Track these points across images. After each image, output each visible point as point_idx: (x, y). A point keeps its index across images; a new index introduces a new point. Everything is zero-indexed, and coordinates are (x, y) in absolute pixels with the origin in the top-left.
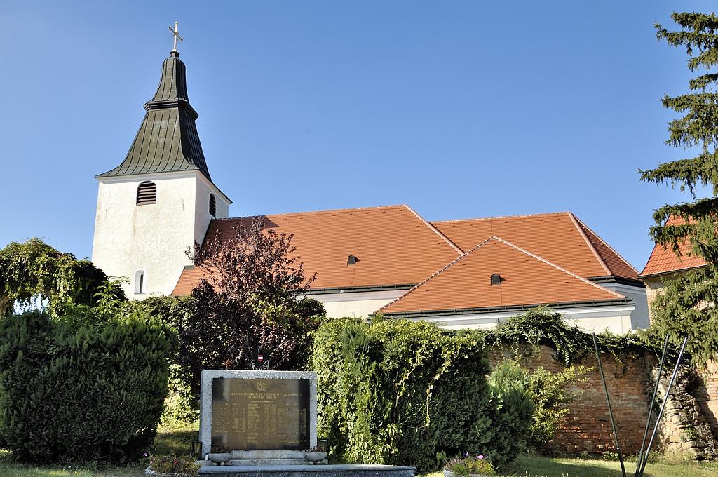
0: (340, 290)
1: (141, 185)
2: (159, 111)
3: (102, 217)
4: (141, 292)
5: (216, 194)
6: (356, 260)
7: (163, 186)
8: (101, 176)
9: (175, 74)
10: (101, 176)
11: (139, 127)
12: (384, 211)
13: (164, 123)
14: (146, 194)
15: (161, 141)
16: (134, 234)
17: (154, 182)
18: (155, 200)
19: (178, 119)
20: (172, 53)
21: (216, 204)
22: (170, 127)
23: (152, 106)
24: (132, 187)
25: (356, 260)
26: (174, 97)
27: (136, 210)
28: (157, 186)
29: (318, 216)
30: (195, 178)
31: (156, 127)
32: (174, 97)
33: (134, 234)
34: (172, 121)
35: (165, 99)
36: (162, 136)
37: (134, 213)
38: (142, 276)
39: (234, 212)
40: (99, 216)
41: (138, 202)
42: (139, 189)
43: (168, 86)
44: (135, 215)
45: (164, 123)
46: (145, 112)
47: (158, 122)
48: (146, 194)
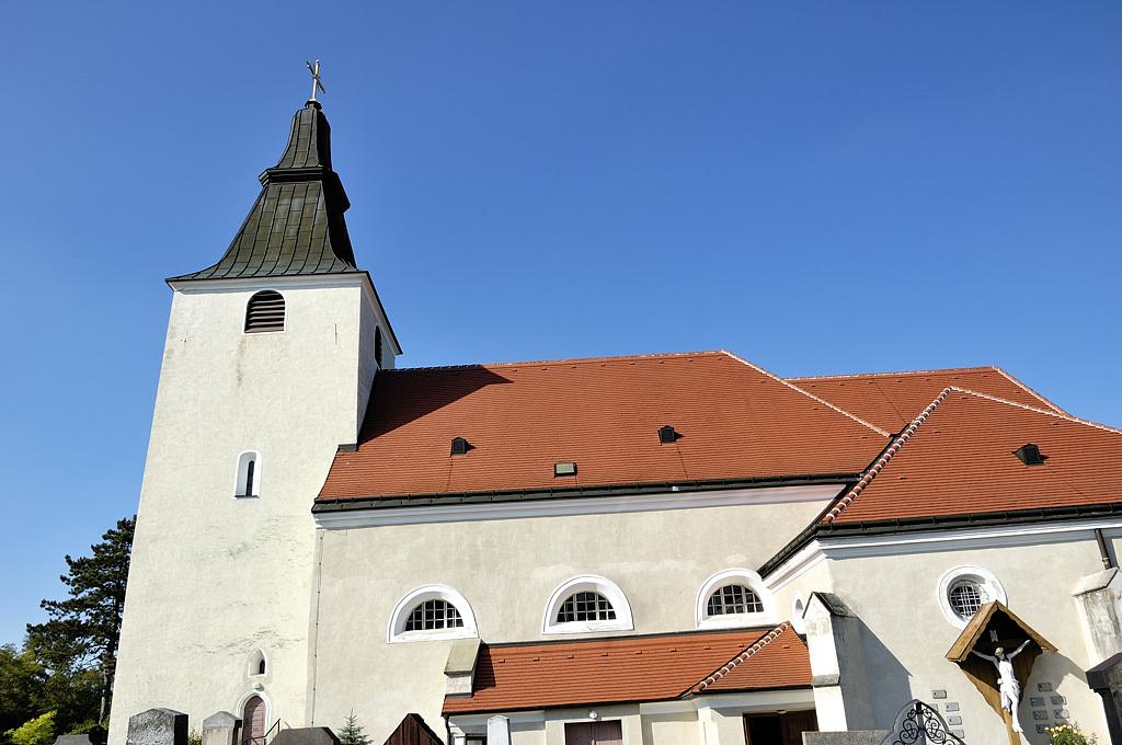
0: (671, 485)
1: (255, 298)
2: (287, 187)
3: (177, 353)
4: (249, 494)
5: (383, 331)
6: (468, 447)
7: (299, 300)
8: (178, 279)
9: (315, 133)
10: (178, 279)
11: (237, 230)
12: (691, 359)
13: (297, 203)
14: (265, 314)
15: (292, 231)
16: (239, 385)
17: (280, 292)
18: (282, 325)
19: (322, 198)
20: (309, 103)
21: (382, 347)
22: (307, 210)
23: (275, 177)
24: (237, 302)
25: (468, 447)
26: (314, 163)
27: (243, 342)
28: (285, 299)
29: (574, 366)
30: (359, 289)
31: (282, 209)
32: (314, 163)
33: (239, 385)
34: (310, 199)
35: (297, 166)
36: (293, 220)
37: (240, 346)
38: (251, 464)
39: (401, 363)
40: (171, 351)
41: (247, 328)
42: (249, 309)
43: (303, 147)
44: (241, 351)
45: (297, 203)
46: (261, 188)
47: (286, 201)
48: (265, 314)
